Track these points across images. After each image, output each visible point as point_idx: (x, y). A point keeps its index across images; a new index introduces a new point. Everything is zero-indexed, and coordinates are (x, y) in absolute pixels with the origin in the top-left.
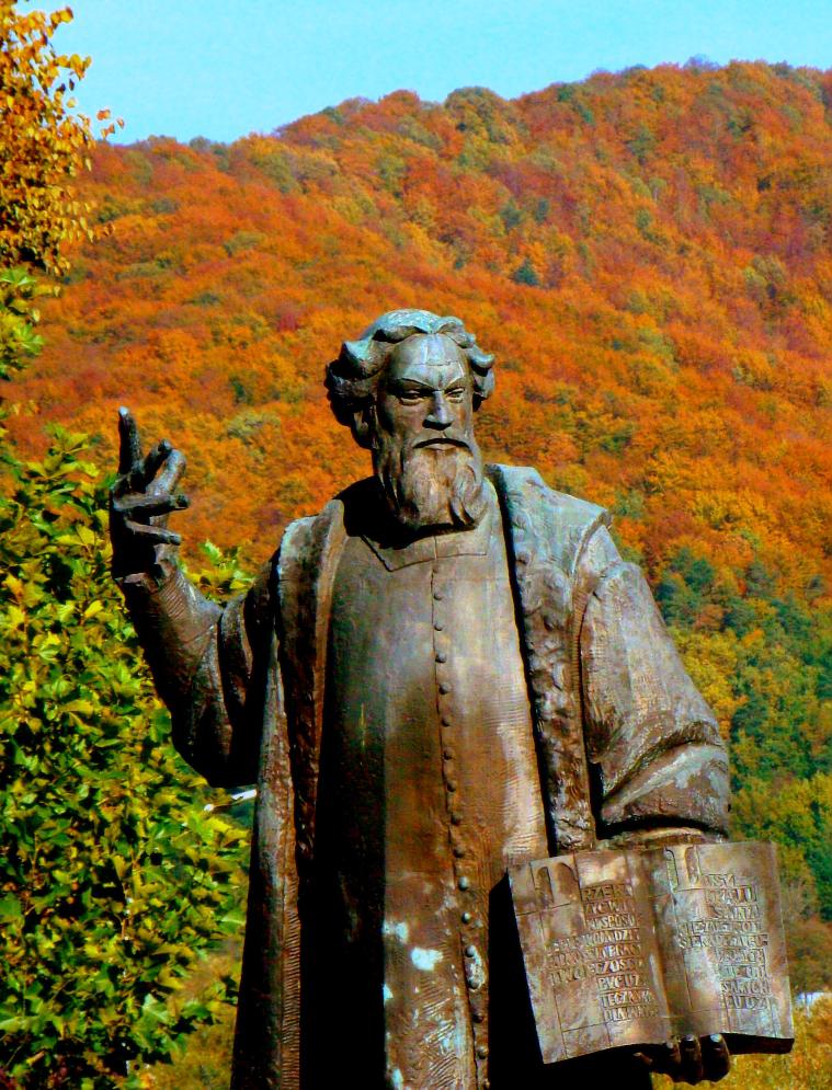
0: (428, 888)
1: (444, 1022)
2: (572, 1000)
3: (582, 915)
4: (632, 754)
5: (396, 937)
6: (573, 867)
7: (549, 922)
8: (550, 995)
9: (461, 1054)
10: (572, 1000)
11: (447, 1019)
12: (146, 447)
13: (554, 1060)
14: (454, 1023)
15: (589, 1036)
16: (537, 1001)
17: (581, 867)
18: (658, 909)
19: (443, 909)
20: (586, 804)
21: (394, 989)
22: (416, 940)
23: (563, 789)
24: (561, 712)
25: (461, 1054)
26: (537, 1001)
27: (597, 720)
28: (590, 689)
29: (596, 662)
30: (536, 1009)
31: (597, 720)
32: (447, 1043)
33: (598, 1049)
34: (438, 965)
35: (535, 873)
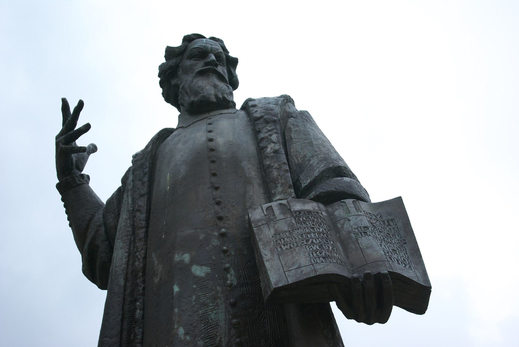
0: (202, 236)
1: (211, 304)
2: (290, 257)
3: (294, 222)
4: (317, 170)
5: (182, 261)
6: (287, 204)
7: (274, 227)
8: (276, 256)
9: (222, 324)
10: (290, 257)
11: (213, 303)
12: (72, 106)
13: (280, 285)
14: (217, 305)
15: (302, 271)
16: (268, 260)
17: (292, 204)
18: (339, 226)
19: (211, 246)
20: (293, 191)
21: (180, 286)
22: (193, 261)
23: (279, 185)
24: (276, 152)
25: (222, 324)
26: (268, 260)
27: (297, 162)
28: (292, 151)
29: (294, 140)
30: (267, 264)
31: (297, 162)
32: (213, 316)
33: (309, 276)
34: (207, 274)
35: (264, 210)
